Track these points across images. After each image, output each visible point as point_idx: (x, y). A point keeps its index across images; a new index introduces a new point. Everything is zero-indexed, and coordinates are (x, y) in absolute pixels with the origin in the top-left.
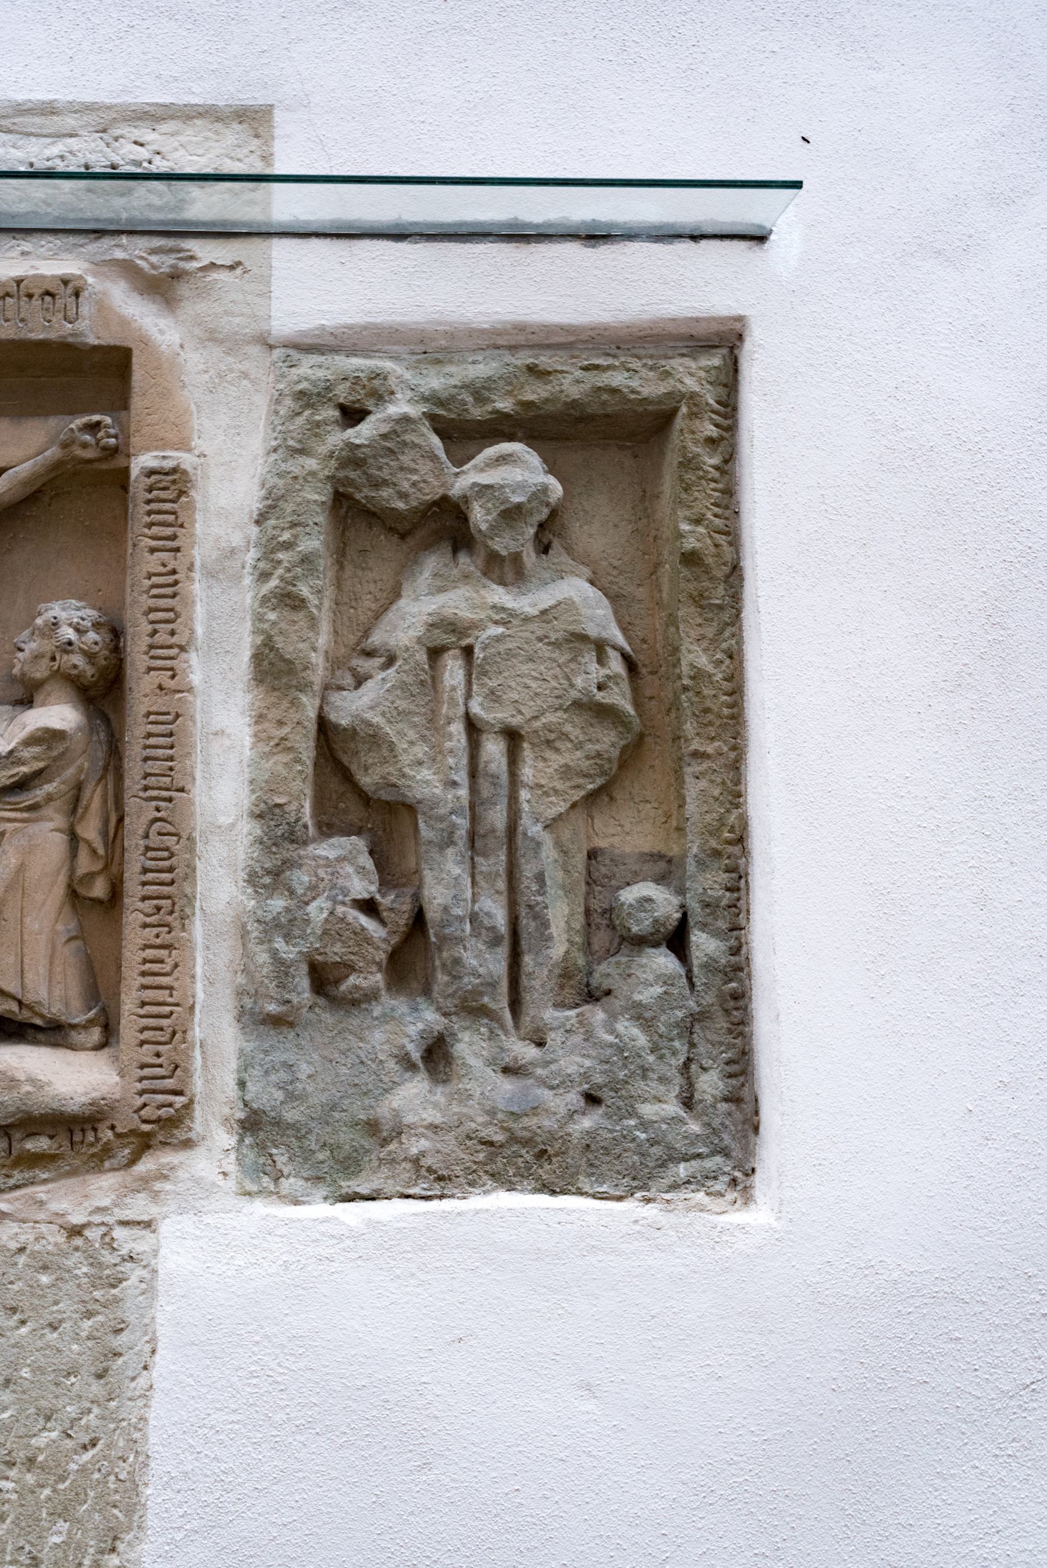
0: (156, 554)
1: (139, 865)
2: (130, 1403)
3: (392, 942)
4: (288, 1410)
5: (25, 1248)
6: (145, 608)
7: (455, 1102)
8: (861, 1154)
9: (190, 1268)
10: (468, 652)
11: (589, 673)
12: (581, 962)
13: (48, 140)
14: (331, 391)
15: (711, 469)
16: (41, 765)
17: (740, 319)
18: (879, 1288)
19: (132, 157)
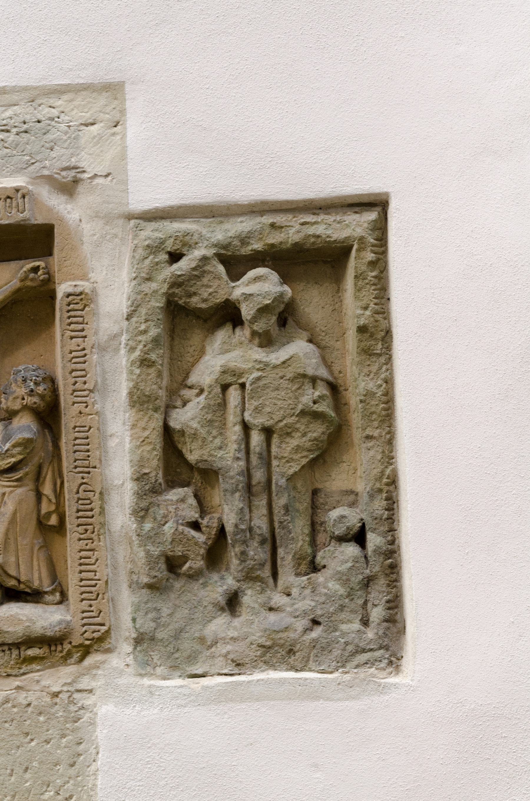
0: (74, 339)
1: (75, 508)
2: (87, 778)
3: (209, 544)
4: (166, 780)
5: (30, 704)
6: (70, 370)
7: (244, 626)
8: (455, 646)
9: (114, 711)
10: (243, 386)
11: (308, 396)
12: (309, 551)
13: (4, 108)
14: (163, 244)
15: (372, 279)
16: (21, 457)
17: (387, 194)
18: (464, 713)
19: (49, 115)
